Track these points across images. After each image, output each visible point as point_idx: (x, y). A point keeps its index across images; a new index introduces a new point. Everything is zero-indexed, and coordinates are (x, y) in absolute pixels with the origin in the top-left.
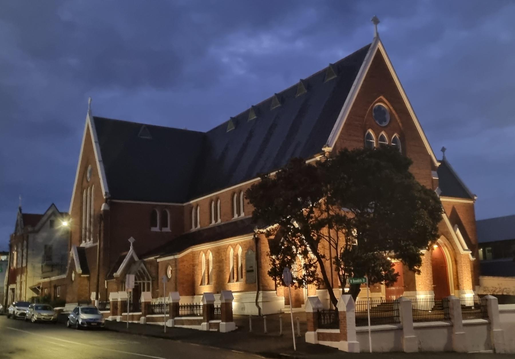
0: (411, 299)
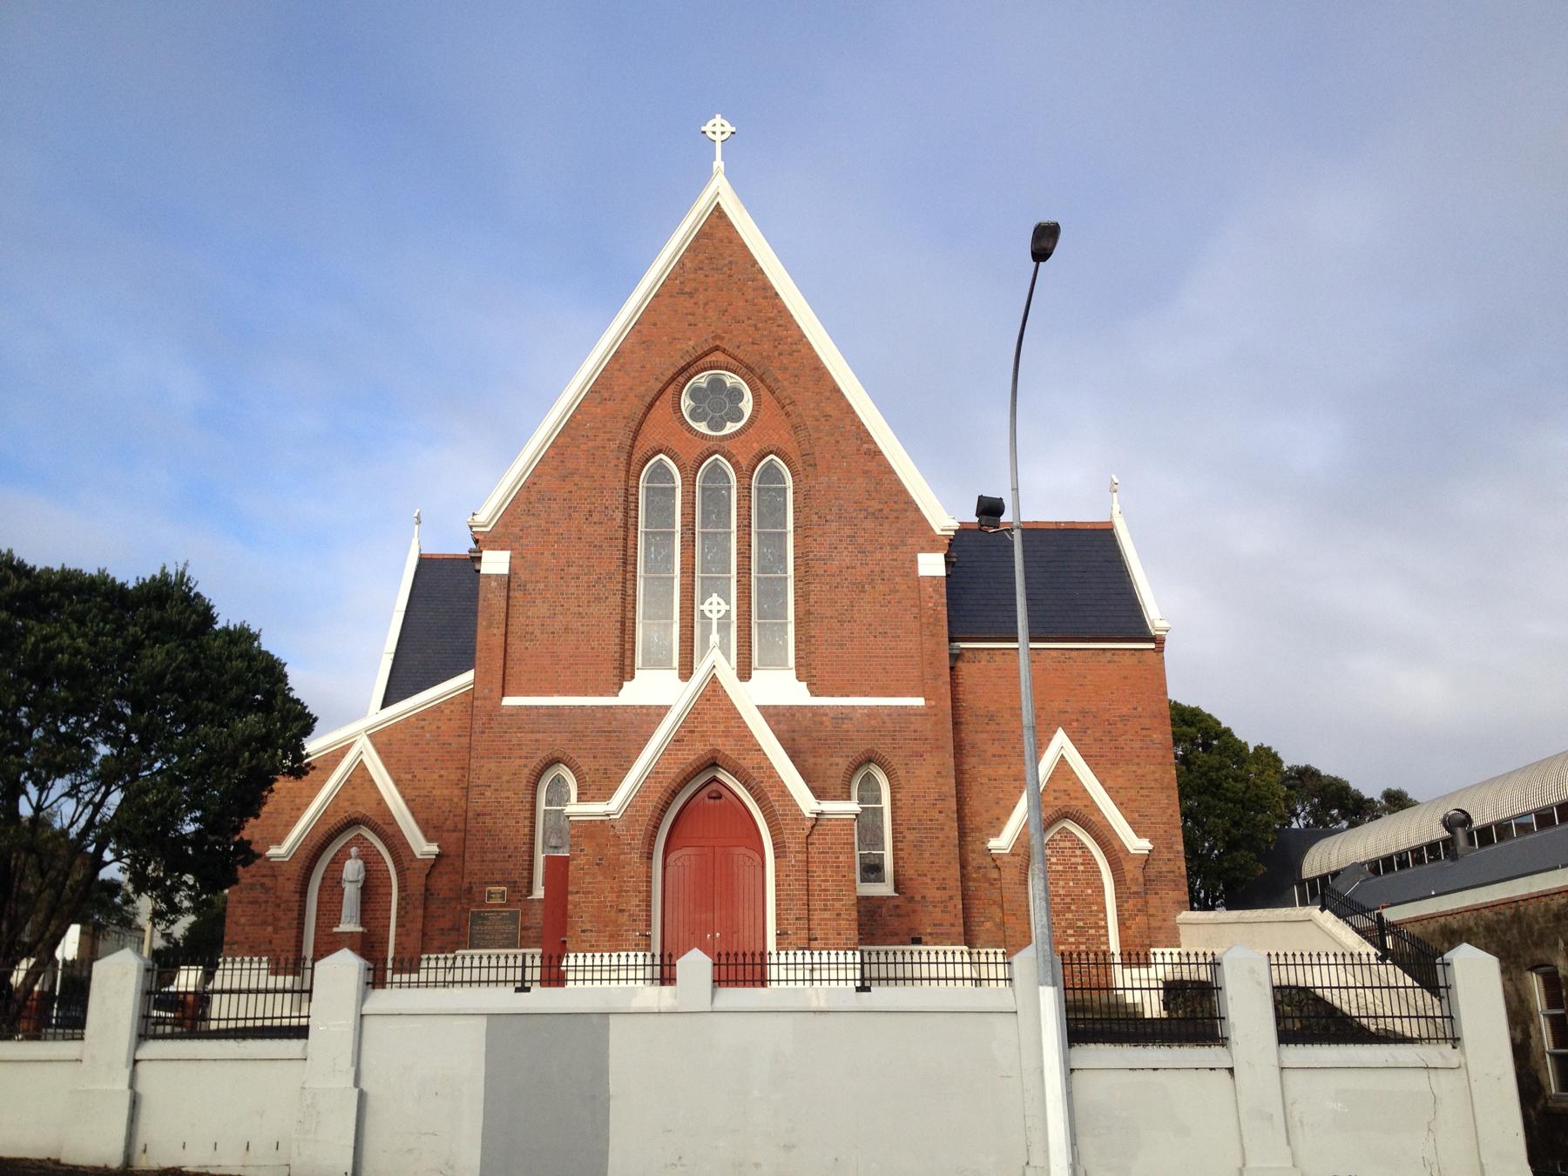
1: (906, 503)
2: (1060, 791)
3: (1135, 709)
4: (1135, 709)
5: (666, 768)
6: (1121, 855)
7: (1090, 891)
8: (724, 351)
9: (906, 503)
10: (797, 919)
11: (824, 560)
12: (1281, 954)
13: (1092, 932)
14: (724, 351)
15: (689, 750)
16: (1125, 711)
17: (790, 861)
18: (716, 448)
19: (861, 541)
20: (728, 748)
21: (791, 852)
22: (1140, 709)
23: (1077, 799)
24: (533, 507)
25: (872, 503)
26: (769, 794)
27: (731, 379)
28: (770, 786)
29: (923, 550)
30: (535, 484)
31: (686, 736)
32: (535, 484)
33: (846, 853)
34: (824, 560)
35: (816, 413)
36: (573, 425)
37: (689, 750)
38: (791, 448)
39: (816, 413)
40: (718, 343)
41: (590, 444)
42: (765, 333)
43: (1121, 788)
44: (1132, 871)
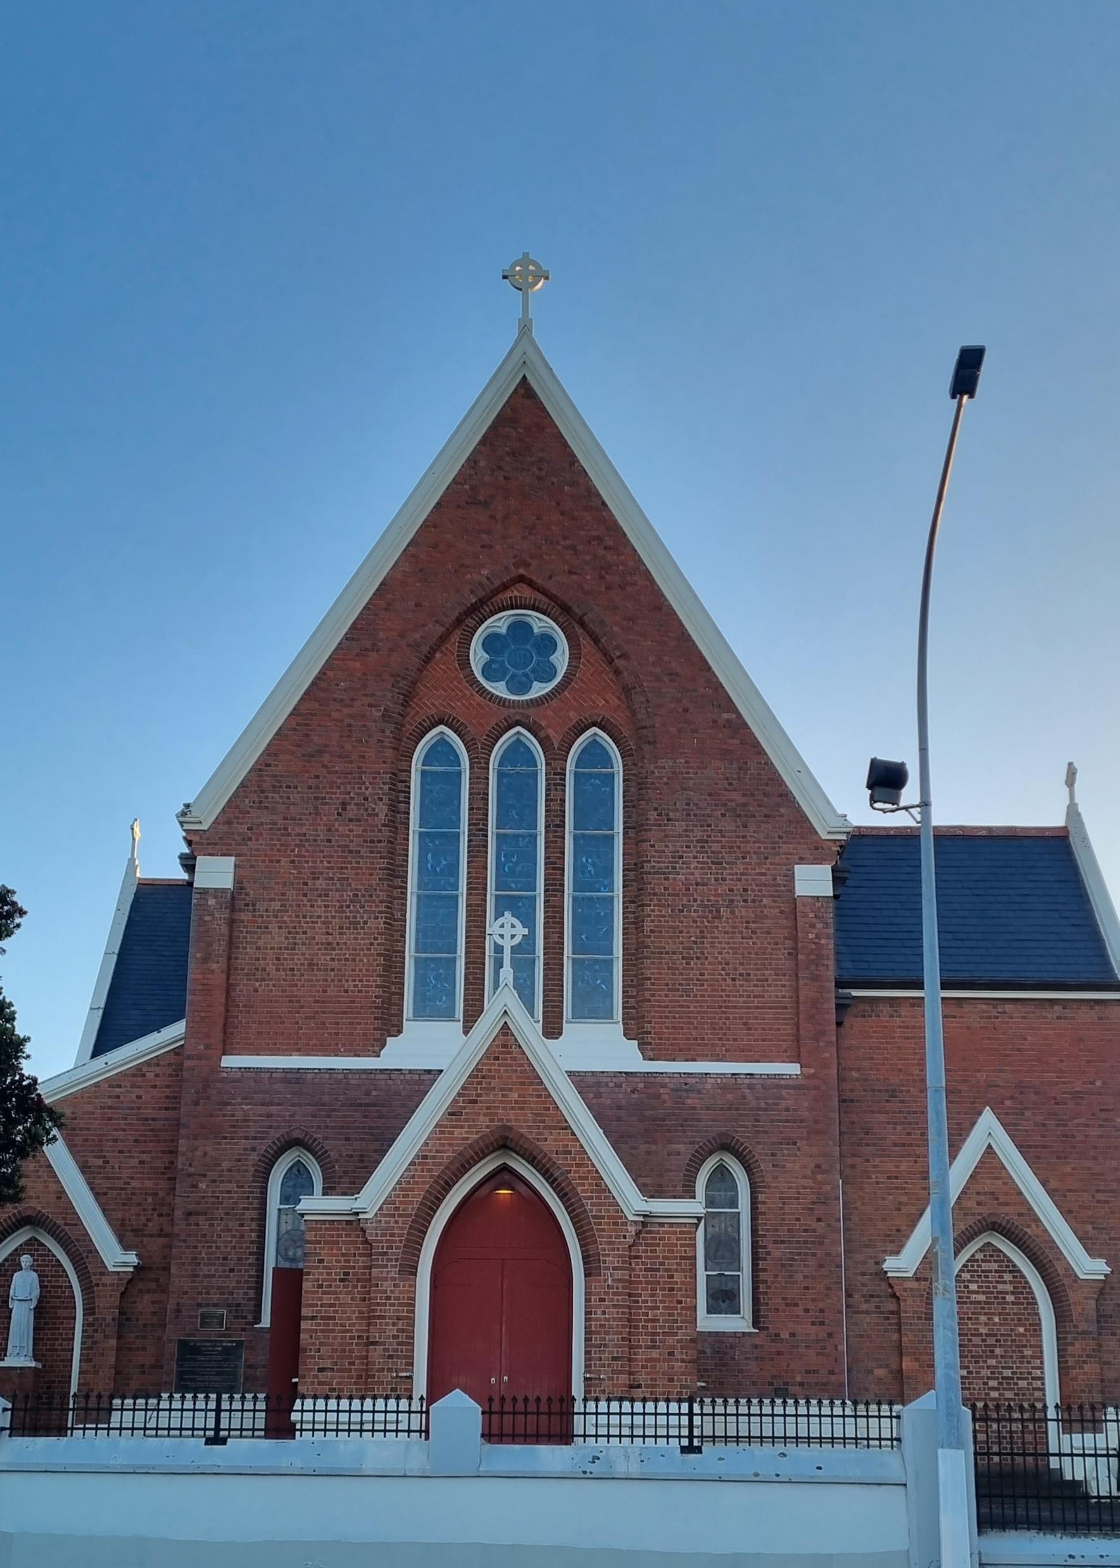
0: (520, 1398)
1: (781, 795)
2: (985, 1193)
3: (1092, 1083)
4: (1092, 1083)
5: (437, 1152)
6: (1066, 1281)
7: (1021, 1330)
8: (530, 583)
9: (781, 795)
10: (614, 1359)
11: (664, 873)
12: (520, 1398)
13: (1023, 1384)
14: (530, 583)
15: (469, 1127)
16: (1078, 1086)
17: (606, 1281)
18: (518, 717)
19: (716, 847)
20: (523, 1125)
21: (607, 1268)
22: (1098, 1083)
23: (1007, 1204)
24: (266, 797)
25: (734, 795)
26: (579, 1189)
27: (540, 623)
28: (580, 1178)
29: (802, 860)
30: (268, 765)
31: (464, 1108)
32: (268, 765)
33: (683, 1271)
34: (664, 873)
35: (658, 670)
36: (323, 685)
37: (469, 1127)
38: (619, 718)
39: (658, 670)
40: (522, 571)
41: (346, 711)
42: (588, 558)
43: (1069, 1191)
44: (1083, 1306)
